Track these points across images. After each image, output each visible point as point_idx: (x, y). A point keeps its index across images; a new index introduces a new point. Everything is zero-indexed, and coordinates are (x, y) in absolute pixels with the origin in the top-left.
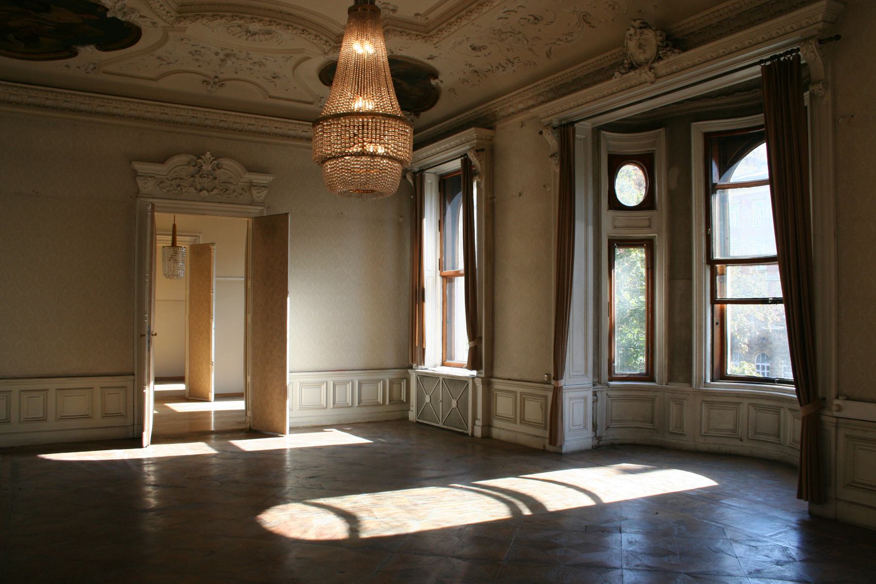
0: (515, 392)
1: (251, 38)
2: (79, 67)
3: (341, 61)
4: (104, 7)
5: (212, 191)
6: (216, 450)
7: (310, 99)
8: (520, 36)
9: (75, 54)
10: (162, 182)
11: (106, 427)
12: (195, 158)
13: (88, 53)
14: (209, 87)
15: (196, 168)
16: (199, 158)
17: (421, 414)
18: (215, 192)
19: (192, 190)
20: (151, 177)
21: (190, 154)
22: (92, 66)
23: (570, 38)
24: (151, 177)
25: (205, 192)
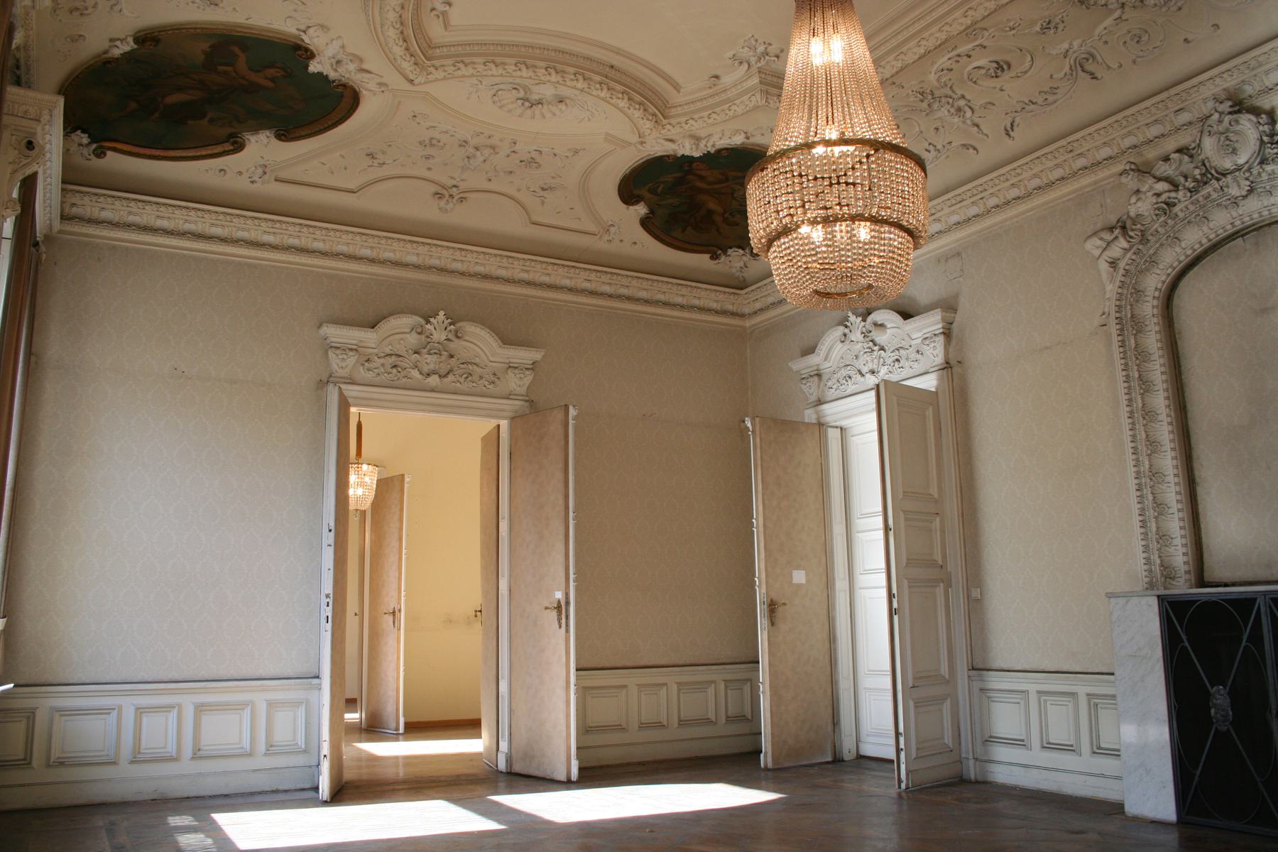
0: (1073, 695)
1: (529, 112)
2: (240, 173)
3: (790, 70)
4: (307, 50)
5: (445, 376)
6: (214, 822)
7: (592, 228)
8: (962, 103)
9: (239, 147)
10: (368, 360)
11: (1046, 769)
12: (423, 322)
13: (262, 148)
14: (442, 203)
15: (423, 337)
16: (428, 322)
17: (509, 760)
18: (451, 377)
19: (415, 373)
20: (351, 350)
21: (416, 314)
22: (260, 171)
23: (1051, 98)
24: (351, 350)
25: (436, 377)
